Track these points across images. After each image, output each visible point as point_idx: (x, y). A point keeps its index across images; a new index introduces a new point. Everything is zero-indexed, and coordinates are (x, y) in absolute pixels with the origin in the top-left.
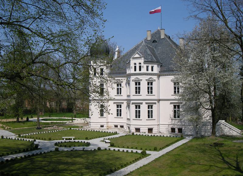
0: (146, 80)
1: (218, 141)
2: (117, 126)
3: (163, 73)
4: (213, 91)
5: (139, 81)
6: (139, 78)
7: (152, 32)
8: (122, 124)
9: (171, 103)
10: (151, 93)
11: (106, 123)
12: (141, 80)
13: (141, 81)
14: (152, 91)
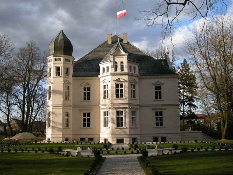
0: (153, 84)
1: (215, 141)
2: (85, 138)
3: (142, 77)
4: (26, 97)
5: (161, 84)
6: (161, 82)
7: (112, 36)
8: (164, 136)
9: (153, 109)
10: (160, 98)
11: (139, 136)
12: (163, 84)
13: (163, 85)
14: (156, 94)
